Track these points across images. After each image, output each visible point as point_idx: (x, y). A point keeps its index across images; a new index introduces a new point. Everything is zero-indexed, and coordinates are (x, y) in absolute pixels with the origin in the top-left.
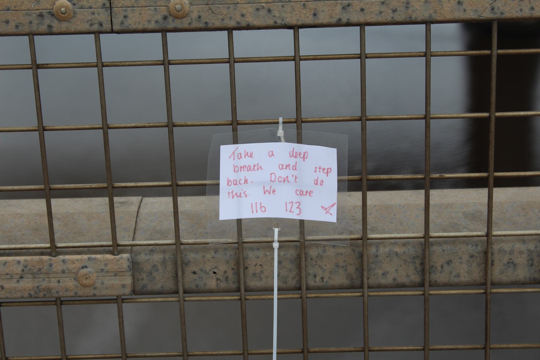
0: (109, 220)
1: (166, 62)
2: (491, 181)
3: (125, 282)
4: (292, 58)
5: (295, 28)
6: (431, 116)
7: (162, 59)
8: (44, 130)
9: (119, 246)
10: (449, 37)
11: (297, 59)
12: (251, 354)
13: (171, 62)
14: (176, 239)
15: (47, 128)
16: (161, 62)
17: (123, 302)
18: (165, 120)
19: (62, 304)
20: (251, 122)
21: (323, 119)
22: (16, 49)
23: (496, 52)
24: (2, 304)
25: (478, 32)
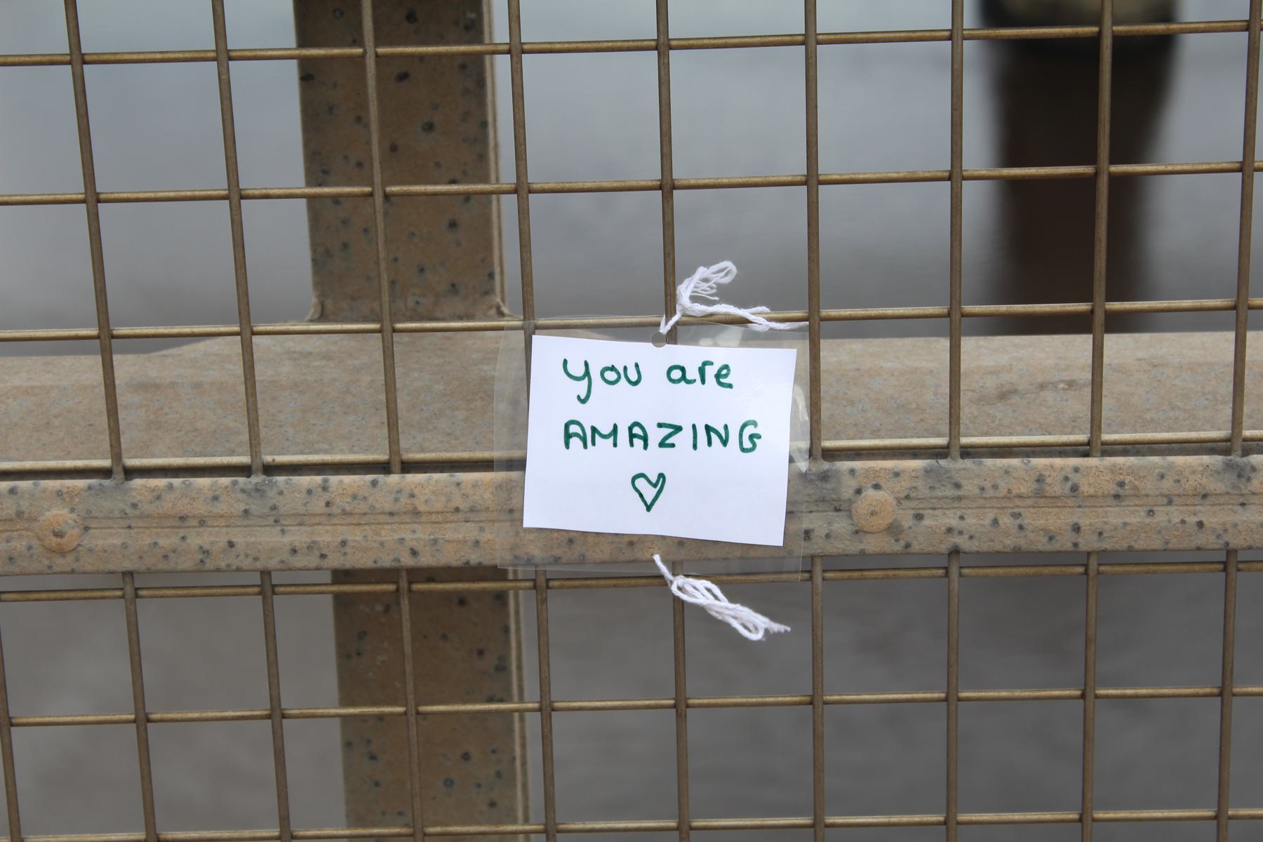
0: (946, 389)
2: (1099, 318)
4: (947, 34)
6: (1256, 165)
12: (290, 717)
13: (87, 58)
14: (1233, 428)
17: (274, 593)
18: (801, 169)
19: (137, 596)
21: (197, 193)
23: (370, 50)
24: (3, 596)
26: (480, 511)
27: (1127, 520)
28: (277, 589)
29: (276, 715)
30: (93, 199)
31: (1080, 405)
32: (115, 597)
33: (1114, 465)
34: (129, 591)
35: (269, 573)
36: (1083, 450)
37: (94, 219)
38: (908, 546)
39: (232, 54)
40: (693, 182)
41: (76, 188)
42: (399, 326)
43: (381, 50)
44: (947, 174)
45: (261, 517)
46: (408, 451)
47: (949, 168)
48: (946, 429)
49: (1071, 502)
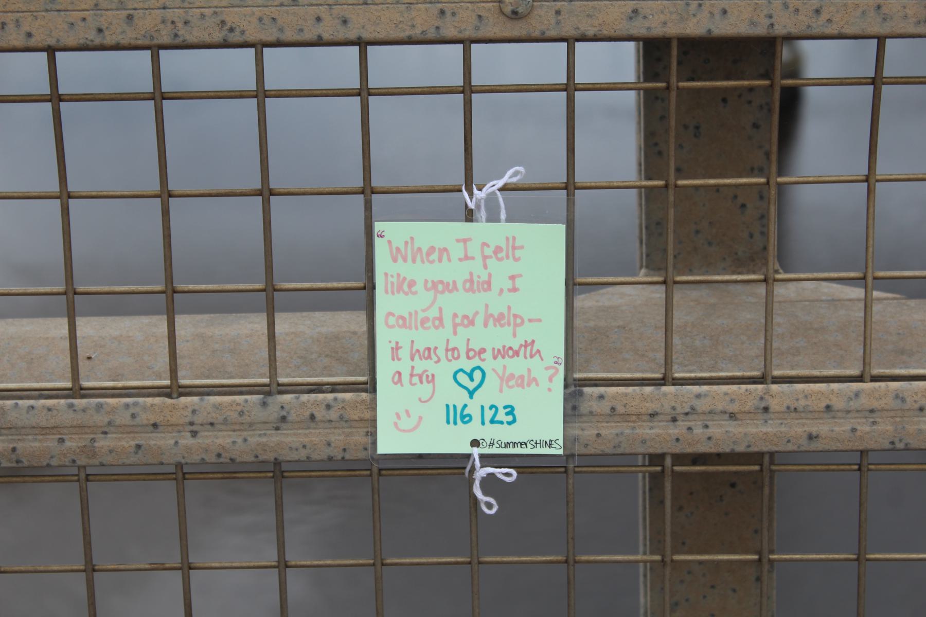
1: (158, 95)
5: (259, 46)
6: (878, 177)
7: (152, 91)
9: (82, 389)
10: (621, 61)
19: (184, 479)
20: (605, 184)
22: (28, 72)
25: (654, 51)
26: (585, 415)
27: (814, 430)
29: (283, 565)
30: (65, 196)
33: (234, 401)
34: (83, 476)
35: (280, 463)
36: (860, 379)
40: (189, 192)
41: (54, 186)
42: (678, 278)
43: (681, 84)
46: (184, 378)
49: (826, 415)
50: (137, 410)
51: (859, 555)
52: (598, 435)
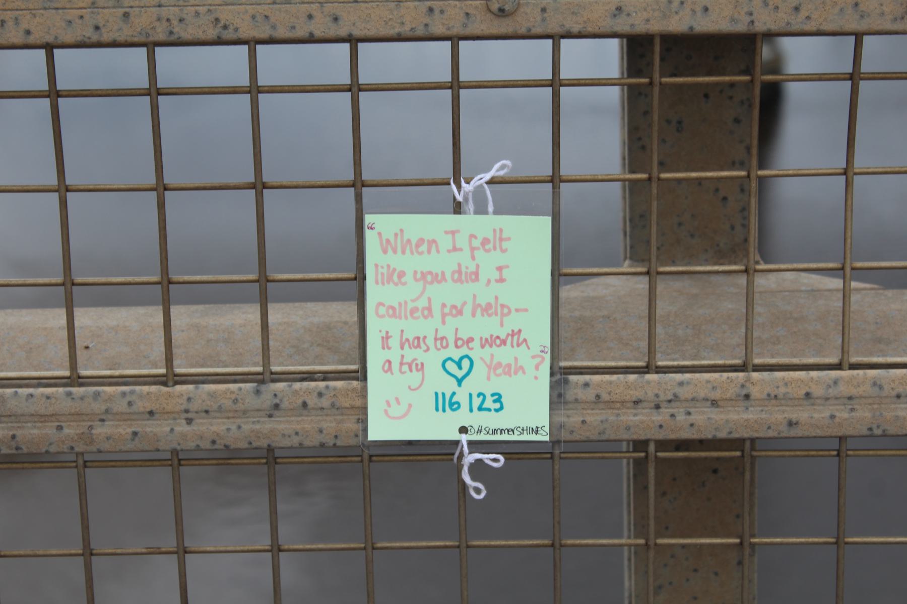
1: (455, 84)
3: (324, 425)
5: (252, 43)
7: (851, 71)
8: (166, 189)
11: (254, 90)
15: (171, 186)
16: (146, 92)
22: (27, 68)
25: (637, 48)
27: (794, 417)
28: (182, 462)
29: (276, 549)
30: (63, 189)
31: (738, 337)
32: (259, 464)
34: (81, 462)
35: (273, 450)
36: (838, 367)
37: (63, 204)
38: (884, 431)
39: (161, 91)
42: (661, 269)
44: (550, 178)
45: (714, 403)
46: (180, 366)
47: (845, 166)
48: (259, 359)
50: (133, 398)
51: (838, 538)
52: (584, 422)
